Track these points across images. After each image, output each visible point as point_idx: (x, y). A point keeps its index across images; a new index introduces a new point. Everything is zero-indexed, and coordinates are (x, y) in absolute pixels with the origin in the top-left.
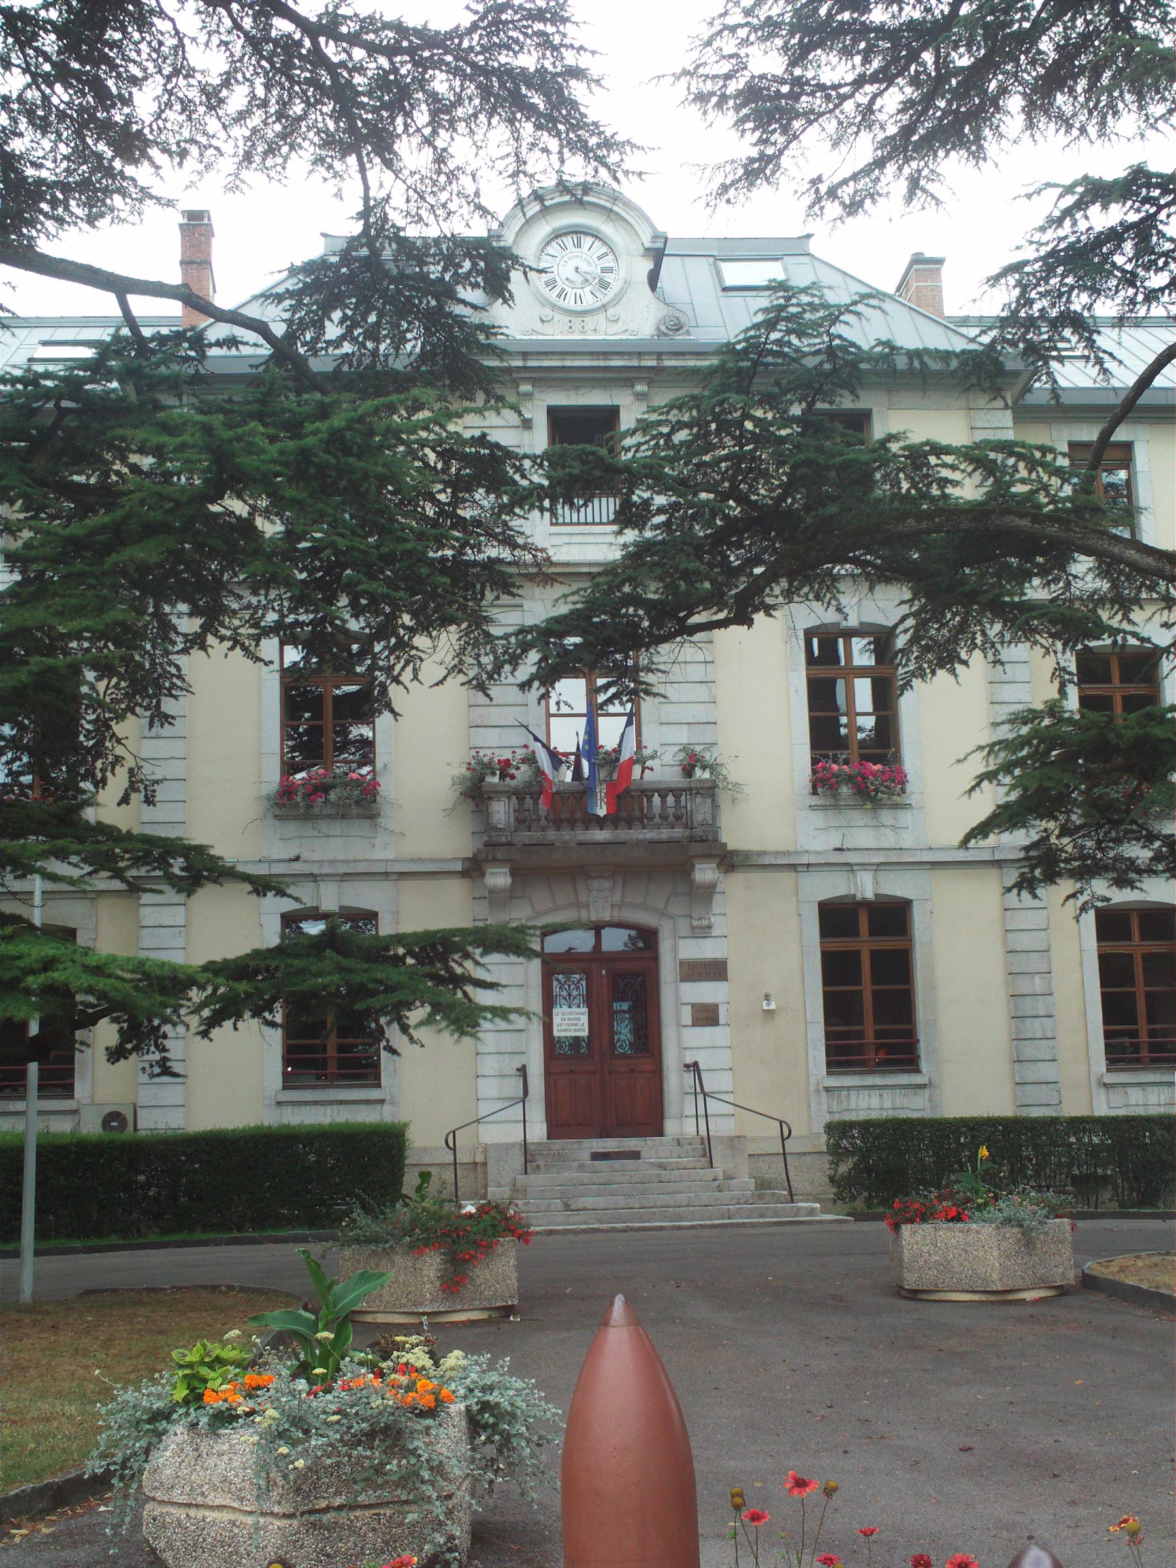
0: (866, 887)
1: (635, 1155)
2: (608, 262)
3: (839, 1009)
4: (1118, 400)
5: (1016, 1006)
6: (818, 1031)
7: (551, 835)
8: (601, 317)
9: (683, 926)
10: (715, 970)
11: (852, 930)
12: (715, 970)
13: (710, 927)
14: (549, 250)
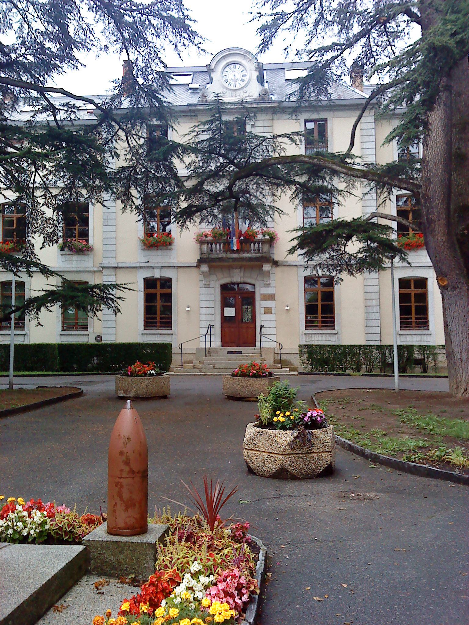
0: (157, 274)
1: (240, 352)
2: (244, 73)
4: (364, 102)
5: (367, 309)
8: (241, 91)
9: (262, 283)
10: (271, 297)
11: (155, 287)
12: (271, 297)
13: (269, 284)
14: (226, 70)
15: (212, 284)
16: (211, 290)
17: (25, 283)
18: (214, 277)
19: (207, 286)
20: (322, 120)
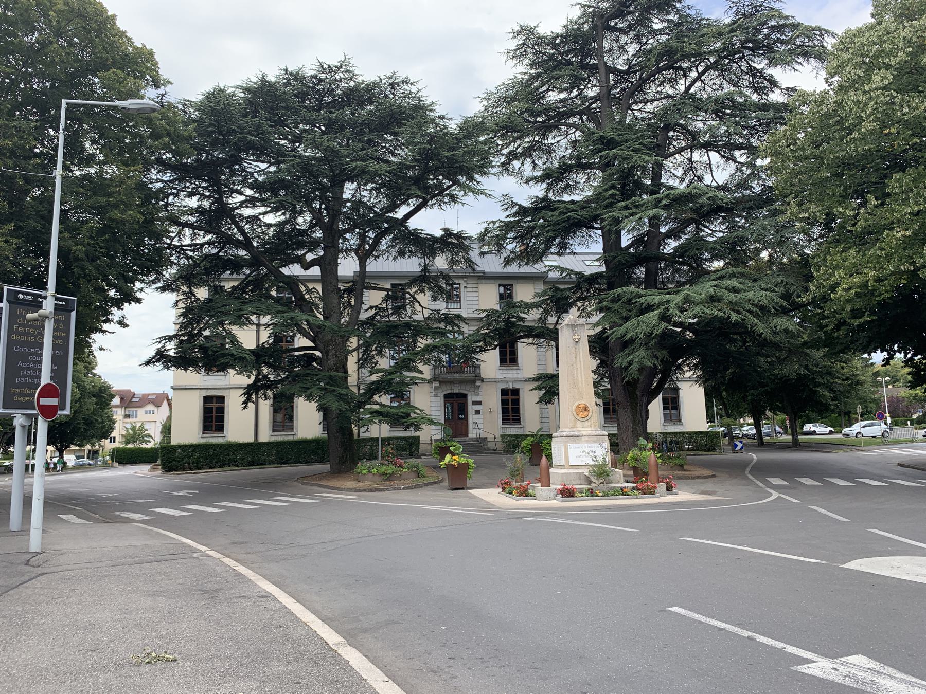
0: (510, 386)
3: (505, 411)
7: (117, 103)
10: (480, 403)
12: (480, 403)
19: (436, 396)
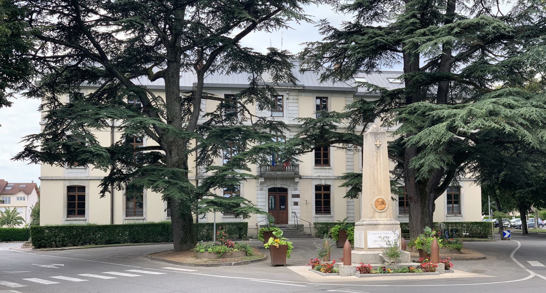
0: (323, 183)
3: (318, 203)
6: (314, 207)
9: (293, 188)
10: (298, 196)
12: (298, 196)
15: (264, 188)
16: (264, 192)
17: (68, 187)
18: (266, 185)
19: (261, 190)
20: (324, 98)
